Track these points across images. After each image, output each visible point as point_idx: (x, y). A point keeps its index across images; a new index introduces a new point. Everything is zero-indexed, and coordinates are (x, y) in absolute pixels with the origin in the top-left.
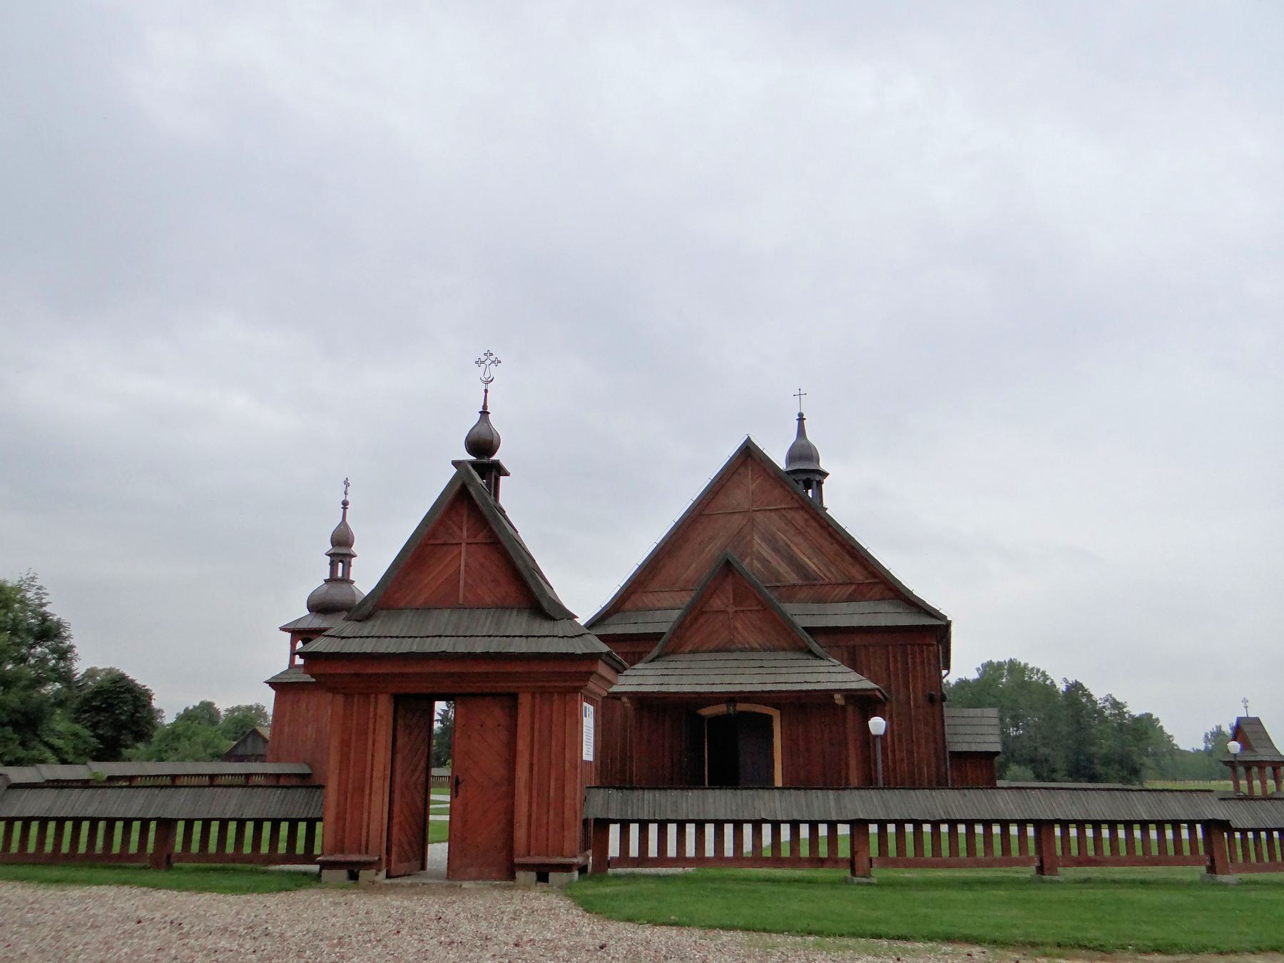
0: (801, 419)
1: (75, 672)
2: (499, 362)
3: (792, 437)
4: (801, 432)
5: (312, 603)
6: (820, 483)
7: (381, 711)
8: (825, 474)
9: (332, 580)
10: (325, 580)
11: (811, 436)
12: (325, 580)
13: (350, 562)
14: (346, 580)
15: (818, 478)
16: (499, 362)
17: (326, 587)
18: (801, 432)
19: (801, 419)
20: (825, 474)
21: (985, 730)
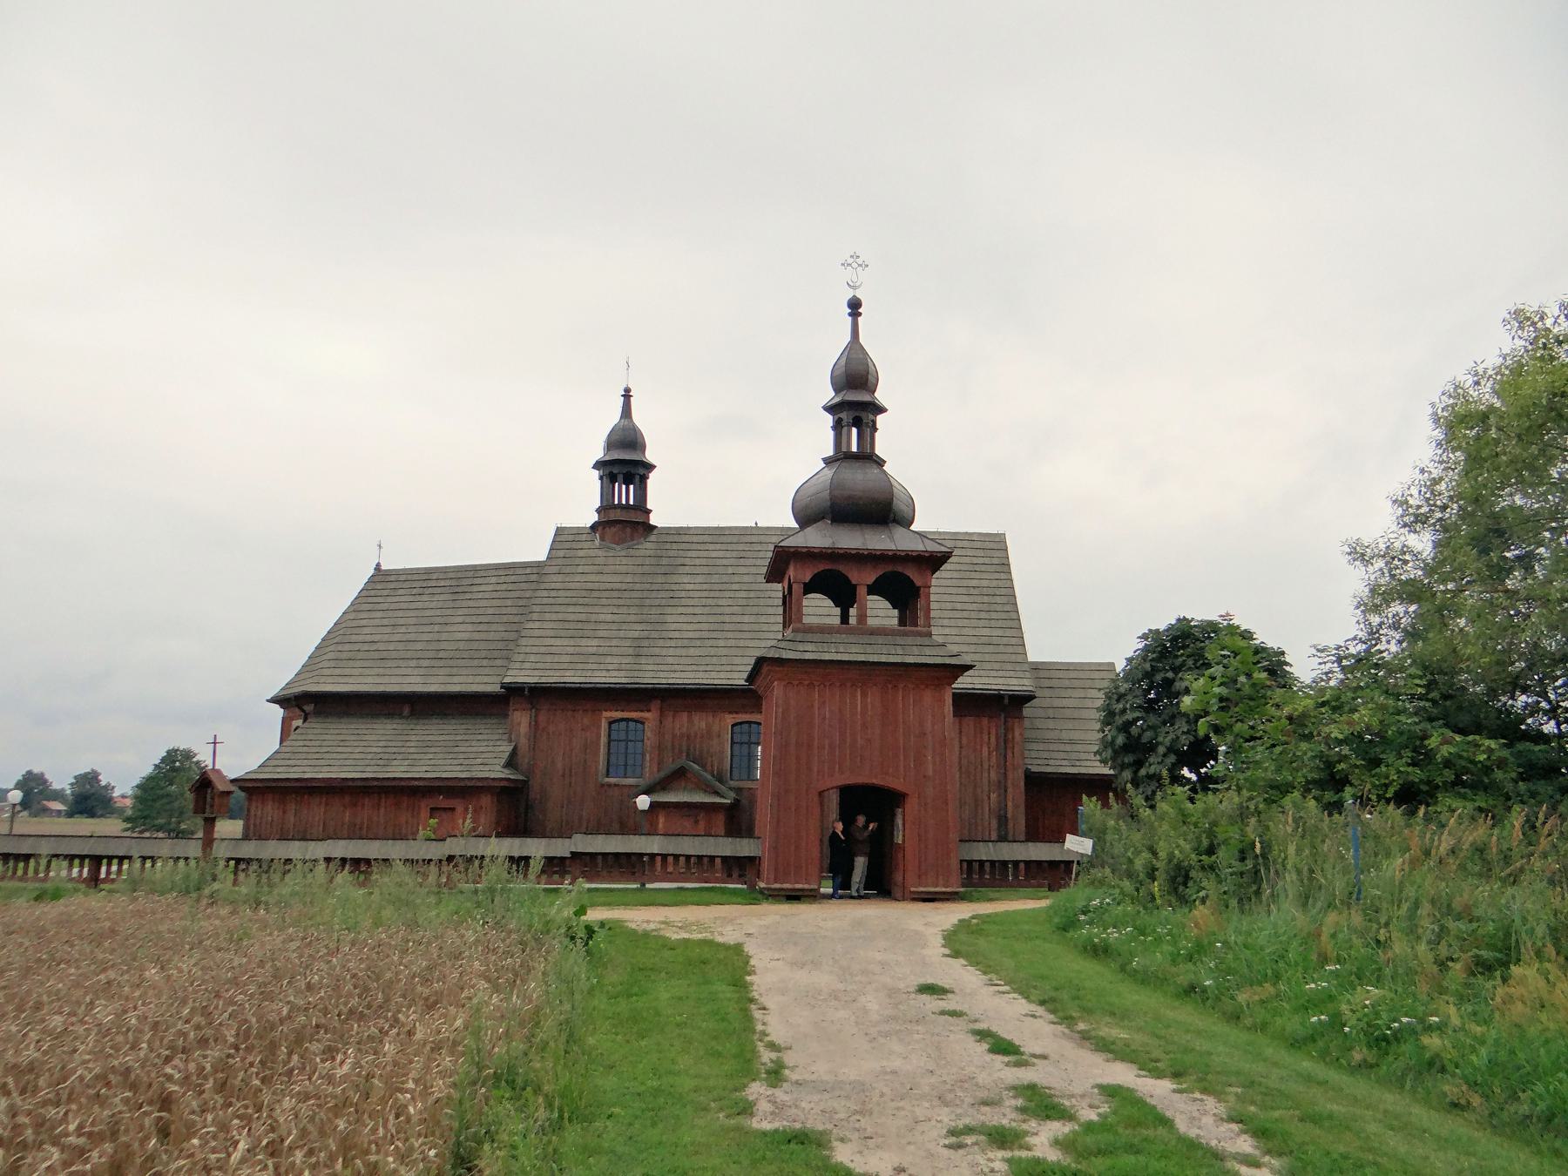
0: (627, 395)
1: (383, 800)
2: (843, 265)
3: (613, 417)
4: (627, 411)
5: (836, 493)
6: (644, 479)
7: (1026, 682)
8: (651, 467)
9: (841, 457)
10: (824, 460)
11: (638, 418)
12: (824, 460)
13: (874, 422)
14: (868, 457)
15: (641, 471)
16: (843, 265)
17: (829, 473)
18: (627, 411)
19: (627, 395)
20: (651, 467)
21: (1085, 714)
